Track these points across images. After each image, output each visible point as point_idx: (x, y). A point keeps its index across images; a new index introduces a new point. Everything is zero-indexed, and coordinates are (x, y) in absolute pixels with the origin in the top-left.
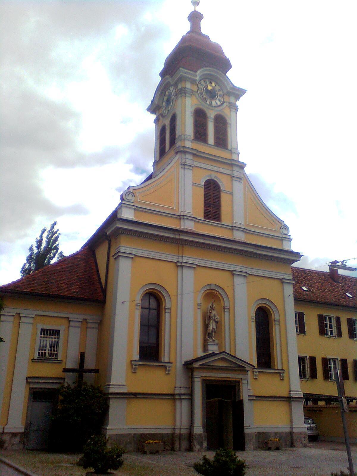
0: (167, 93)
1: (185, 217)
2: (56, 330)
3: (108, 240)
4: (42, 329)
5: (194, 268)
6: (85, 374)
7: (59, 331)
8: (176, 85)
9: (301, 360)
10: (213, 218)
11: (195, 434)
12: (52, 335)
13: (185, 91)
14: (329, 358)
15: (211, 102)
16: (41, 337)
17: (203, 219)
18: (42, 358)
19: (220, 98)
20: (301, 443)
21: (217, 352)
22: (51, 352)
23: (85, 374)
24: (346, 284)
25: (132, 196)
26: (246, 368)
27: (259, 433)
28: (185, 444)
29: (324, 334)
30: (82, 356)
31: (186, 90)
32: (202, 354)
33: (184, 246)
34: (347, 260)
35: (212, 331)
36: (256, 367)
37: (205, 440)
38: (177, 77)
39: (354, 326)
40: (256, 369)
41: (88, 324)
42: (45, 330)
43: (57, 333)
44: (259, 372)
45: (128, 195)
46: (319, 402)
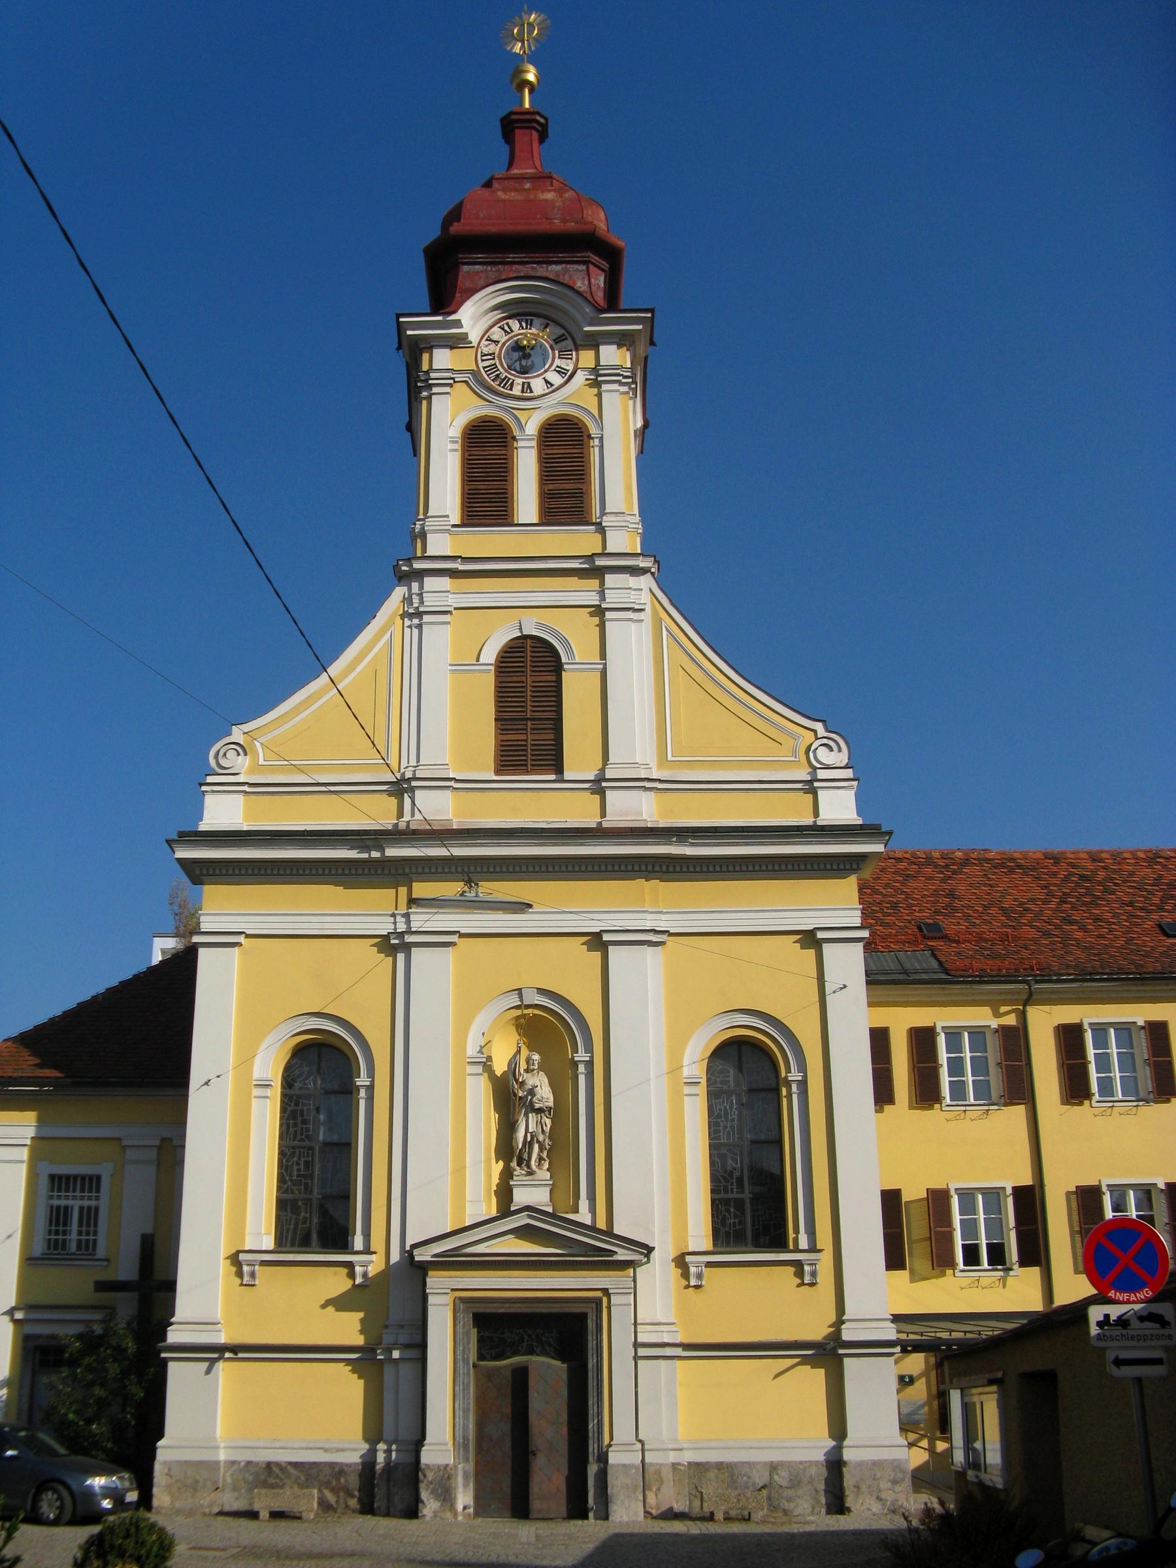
2: (91, 1178)
4: (52, 1177)
5: (662, 943)
7: (99, 1178)
9: (891, 1200)
11: (426, 1465)
12: (67, 1190)
16: (51, 1197)
18: (55, 1254)
22: (88, 1237)
26: (616, 1253)
37: (466, 1485)
41: (128, 1152)
42: (60, 1177)
43: (92, 1183)
44: (709, 1264)
45: (225, 754)
46: (823, 1370)
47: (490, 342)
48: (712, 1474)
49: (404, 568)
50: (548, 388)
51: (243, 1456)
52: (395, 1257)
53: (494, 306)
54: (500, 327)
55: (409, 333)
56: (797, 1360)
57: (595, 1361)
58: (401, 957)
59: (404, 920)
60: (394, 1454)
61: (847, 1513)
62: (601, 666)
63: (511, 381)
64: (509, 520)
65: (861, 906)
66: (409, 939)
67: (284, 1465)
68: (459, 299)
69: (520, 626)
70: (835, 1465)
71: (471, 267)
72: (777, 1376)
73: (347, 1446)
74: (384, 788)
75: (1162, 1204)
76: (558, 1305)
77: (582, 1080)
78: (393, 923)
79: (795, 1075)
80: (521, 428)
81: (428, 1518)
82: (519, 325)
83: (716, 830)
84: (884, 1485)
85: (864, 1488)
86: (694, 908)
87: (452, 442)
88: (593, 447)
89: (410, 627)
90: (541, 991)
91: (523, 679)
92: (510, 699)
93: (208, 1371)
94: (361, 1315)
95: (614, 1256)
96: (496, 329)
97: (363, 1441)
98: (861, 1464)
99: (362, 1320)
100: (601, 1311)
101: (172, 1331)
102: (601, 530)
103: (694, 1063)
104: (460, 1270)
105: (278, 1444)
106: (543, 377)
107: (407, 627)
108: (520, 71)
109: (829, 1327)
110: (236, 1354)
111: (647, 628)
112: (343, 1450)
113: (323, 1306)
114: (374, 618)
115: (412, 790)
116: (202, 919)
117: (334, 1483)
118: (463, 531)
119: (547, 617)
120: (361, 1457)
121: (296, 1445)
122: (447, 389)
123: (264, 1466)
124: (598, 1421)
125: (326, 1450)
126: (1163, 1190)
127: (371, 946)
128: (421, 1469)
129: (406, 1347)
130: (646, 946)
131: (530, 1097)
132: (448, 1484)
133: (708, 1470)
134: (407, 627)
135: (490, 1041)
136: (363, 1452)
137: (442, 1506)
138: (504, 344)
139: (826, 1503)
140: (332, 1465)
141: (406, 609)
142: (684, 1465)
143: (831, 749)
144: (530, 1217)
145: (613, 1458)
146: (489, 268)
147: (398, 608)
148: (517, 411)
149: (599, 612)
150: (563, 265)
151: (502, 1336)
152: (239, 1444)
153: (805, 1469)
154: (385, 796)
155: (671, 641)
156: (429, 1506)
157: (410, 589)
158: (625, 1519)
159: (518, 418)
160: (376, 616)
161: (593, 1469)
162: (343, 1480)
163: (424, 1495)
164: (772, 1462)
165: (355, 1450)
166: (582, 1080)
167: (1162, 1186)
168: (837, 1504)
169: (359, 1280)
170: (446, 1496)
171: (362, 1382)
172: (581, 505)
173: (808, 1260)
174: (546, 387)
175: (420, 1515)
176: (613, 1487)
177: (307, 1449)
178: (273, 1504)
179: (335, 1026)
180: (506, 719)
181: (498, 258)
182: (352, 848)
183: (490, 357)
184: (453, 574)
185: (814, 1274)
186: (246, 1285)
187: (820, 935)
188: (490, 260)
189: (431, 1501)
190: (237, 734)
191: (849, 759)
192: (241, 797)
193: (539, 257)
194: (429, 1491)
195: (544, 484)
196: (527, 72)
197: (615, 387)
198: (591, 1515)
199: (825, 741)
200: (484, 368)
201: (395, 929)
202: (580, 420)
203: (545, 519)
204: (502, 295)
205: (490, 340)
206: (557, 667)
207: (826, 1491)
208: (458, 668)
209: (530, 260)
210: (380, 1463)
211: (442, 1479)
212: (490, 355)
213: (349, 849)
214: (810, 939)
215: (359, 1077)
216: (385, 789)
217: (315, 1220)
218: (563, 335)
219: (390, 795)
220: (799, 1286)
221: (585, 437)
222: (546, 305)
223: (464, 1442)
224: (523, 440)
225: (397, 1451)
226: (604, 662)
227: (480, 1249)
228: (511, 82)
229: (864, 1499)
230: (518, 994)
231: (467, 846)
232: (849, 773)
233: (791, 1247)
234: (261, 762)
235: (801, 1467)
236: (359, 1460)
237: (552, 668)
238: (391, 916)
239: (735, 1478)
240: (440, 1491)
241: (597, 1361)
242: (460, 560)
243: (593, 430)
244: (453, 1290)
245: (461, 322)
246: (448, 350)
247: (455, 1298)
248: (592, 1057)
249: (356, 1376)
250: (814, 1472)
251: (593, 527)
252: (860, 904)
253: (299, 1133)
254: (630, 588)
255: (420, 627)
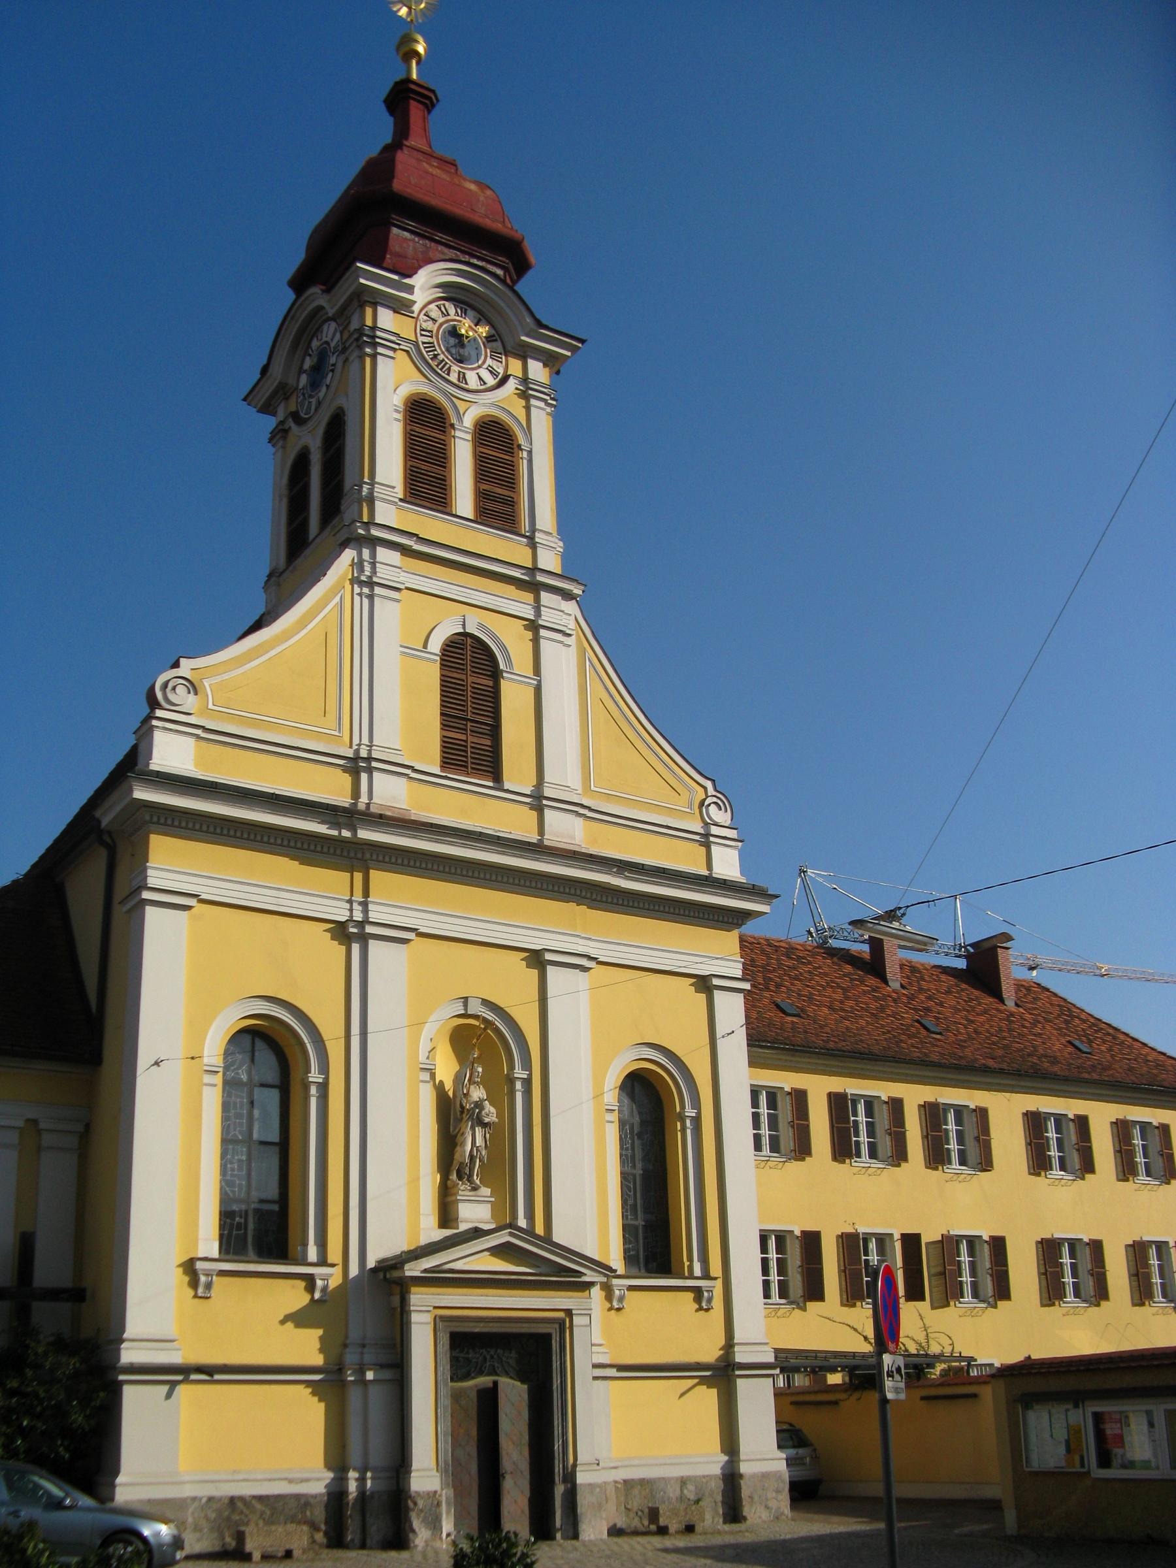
0: (315, 344)
1: (374, 764)
3: (103, 843)
6: (36, 1306)
8: (343, 315)
10: (472, 768)
11: (416, 1492)
13: (374, 337)
14: (863, 1233)
15: (464, 377)
17: (437, 771)
19: (495, 364)
20: (767, 1507)
21: (486, 1227)
23: (36, 1306)
24: (921, 990)
25: (189, 693)
27: (628, 1484)
28: (378, 1528)
29: (850, 1157)
30: (26, 1245)
31: (379, 333)
32: (440, 1234)
33: (371, 864)
34: (908, 907)
35: (472, 1157)
36: (618, 1273)
37: (448, 1513)
38: (343, 292)
39: (944, 1127)
40: (619, 1277)
44: (631, 1288)
45: (174, 688)
47: (428, 319)
48: (636, 1491)
49: (361, 531)
50: (481, 385)
51: (205, 1491)
52: (354, 1271)
53: (438, 283)
54: (437, 306)
55: (362, 281)
56: (696, 1381)
57: (559, 1382)
58: (356, 948)
59: (360, 908)
60: (369, 1483)
61: (743, 1521)
62: (535, 682)
63: (448, 366)
64: (448, 510)
65: (743, 960)
66: (369, 929)
67: (248, 1499)
68: (390, 261)
69: (464, 622)
70: (731, 1479)
71: (400, 231)
72: (682, 1395)
73: (619, 1464)
74: (341, 762)
75: (797, 1249)
76: (526, 1325)
77: (519, 1097)
78: (349, 910)
79: (690, 1112)
80: (460, 420)
81: (420, 1548)
82: (455, 311)
83: (643, 867)
84: (771, 1494)
85: (756, 1498)
86: (612, 939)
87: (397, 411)
88: (522, 458)
89: (359, 594)
90: (486, 1003)
91: (463, 677)
92: (452, 695)
93: (169, 1395)
94: (320, 1332)
95: (582, 1277)
96: (433, 306)
97: (326, 1470)
98: (754, 1476)
99: (321, 1338)
100: (564, 1332)
101: (127, 1349)
102: (533, 545)
103: (611, 1090)
104: (503, 1289)
105: (240, 1477)
106: (477, 371)
107: (357, 594)
108: (407, 40)
109: (720, 1349)
110: (211, 1375)
111: (572, 653)
112: (307, 1480)
113: (283, 1322)
114: (324, 576)
115: (370, 771)
116: (150, 872)
117: (300, 1517)
118: (408, 508)
119: (490, 620)
120: (326, 1487)
121: (260, 1477)
122: (390, 353)
123: (226, 1501)
124: (563, 1441)
125: (291, 1481)
126: (798, 1237)
127: (324, 931)
128: (410, 1497)
129: (380, 1366)
130: (578, 970)
131: (477, 1110)
132: (438, 1511)
133: (632, 1487)
134: (357, 594)
135: (434, 1048)
136: (328, 1481)
137: (433, 1534)
138: (441, 325)
139: (723, 1513)
140: (297, 1497)
141: (356, 575)
142: (619, 1483)
143: (720, 809)
144: (511, 1234)
145: (581, 1478)
146: (417, 239)
147: (346, 574)
148: (459, 401)
149: (533, 626)
150: (484, 263)
151: (467, 1356)
152: (197, 1478)
153: (707, 1482)
154: (339, 771)
155: (592, 669)
156: (420, 1536)
157: (360, 554)
158: (592, 1537)
159: (455, 405)
160: (326, 574)
161: (559, 1490)
162: (308, 1513)
163: (416, 1524)
164: (682, 1477)
165: (318, 1479)
166: (519, 1097)
167: (797, 1233)
168: (733, 1512)
169: (317, 1295)
170: (434, 1524)
171: (322, 1405)
172: (513, 514)
173: (707, 1287)
174: (479, 384)
175: (412, 1545)
176: (582, 1506)
177: (270, 1480)
178: (265, 1544)
179: (286, 1014)
180: (451, 716)
181: (428, 232)
182: (323, 822)
183: (428, 334)
184: (406, 551)
185: (710, 1300)
186: (201, 1297)
187: (716, 982)
188: (418, 231)
189: (423, 1529)
190: (187, 667)
191: (732, 820)
192: (191, 741)
193: (465, 246)
194: (420, 1519)
195: (479, 482)
196: (418, 42)
197: (542, 404)
198: (558, 1535)
199: (715, 800)
200: (424, 343)
201: (351, 916)
202: (510, 427)
203: (480, 518)
204: (440, 275)
205: (428, 316)
206: (495, 674)
207: (723, 1502)
208: (408, 651)
209: (456, 246)
210: (353, 1493)
211: (432, 1506)
212: (429, 331)
213: (319, 823)
214: (704, 984)
215: (310, 1073)
216: (341, 764)
217: (251, 1226)
218: (494, 336)
219: (345, 771)
220: (697, 1310)
221: (516, 450)
222: (483, 299)
223: (445, 1467)
224: (460, 430)
225: (372, 1478)
226: (539, 678)
227: (459, 1265)
228: (398, 49)
229: (756, 1508)
230: (463, 1002)
231: (437, 841)
232: (733, 834)
233: (686, 1274)
234: (211, 706)
235: (704, 1480)
236: (324, 1491)
237: (489, 673)
238: (347, 902)
239: (654, 1493)
240: (430, 1519)
241: (561, 1381)
242: (415, 538)
243: (522, 440)
244: (435, 1308)
245: (413, 289)
246: (391, 312)
247: (435, 1316)
248: (530, 1075)
249: (316, 1399)
250: (713, 1485)
251: (525, 540)
252: (741, 958)
253: (232, 1127)
254: (562, 611)
255: (371, 597)
